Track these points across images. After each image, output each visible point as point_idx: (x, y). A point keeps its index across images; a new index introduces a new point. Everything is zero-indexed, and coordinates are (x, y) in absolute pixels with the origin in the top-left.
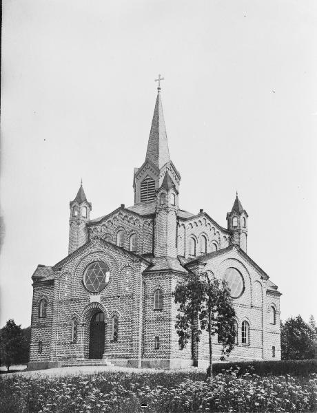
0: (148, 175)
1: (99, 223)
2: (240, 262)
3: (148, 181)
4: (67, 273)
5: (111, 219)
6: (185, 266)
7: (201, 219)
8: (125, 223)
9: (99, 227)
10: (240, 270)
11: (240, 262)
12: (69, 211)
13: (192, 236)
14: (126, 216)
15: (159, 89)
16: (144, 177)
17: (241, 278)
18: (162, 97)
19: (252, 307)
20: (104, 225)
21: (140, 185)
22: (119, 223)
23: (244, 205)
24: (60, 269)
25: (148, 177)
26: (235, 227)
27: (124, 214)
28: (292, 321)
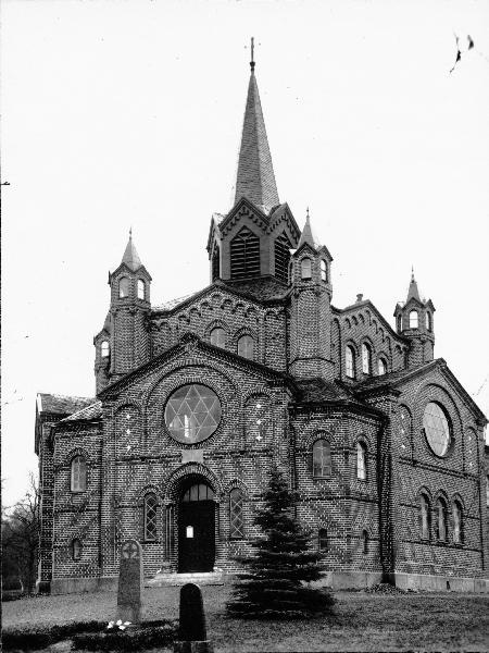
0: (245, 227)
1: (172, 313)
2: (446, 392)
3: (245, 238)
4: (127, 405)
5: (198, 305)
6: (356, 396)
7: (363, 312)
8: (226, 314)
9: (173, 321)
10: (443, 403)
11: (446, 392)
12: (108, 289)
13: (349, 343)
14: (229, 301)
15: (252, 64)
16: (236, 230)
17: (445, 423)
18: (260, 83)
19: (466, 475)
20: (183, 316)
21: (228, 245)
22: (215, 315)
23: (144, 258)
24: (115, 398)
25: (245, 231)
26: (414, 329)
27: (248, 306)
28: (56, 627)
